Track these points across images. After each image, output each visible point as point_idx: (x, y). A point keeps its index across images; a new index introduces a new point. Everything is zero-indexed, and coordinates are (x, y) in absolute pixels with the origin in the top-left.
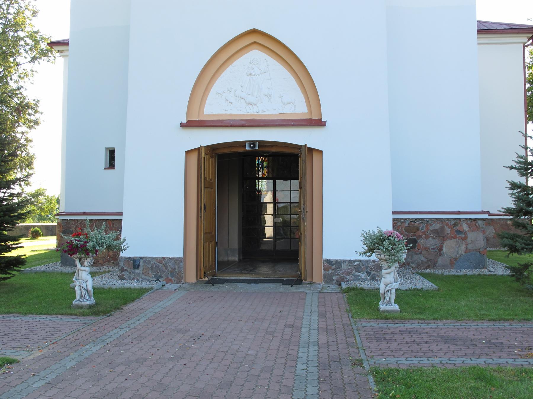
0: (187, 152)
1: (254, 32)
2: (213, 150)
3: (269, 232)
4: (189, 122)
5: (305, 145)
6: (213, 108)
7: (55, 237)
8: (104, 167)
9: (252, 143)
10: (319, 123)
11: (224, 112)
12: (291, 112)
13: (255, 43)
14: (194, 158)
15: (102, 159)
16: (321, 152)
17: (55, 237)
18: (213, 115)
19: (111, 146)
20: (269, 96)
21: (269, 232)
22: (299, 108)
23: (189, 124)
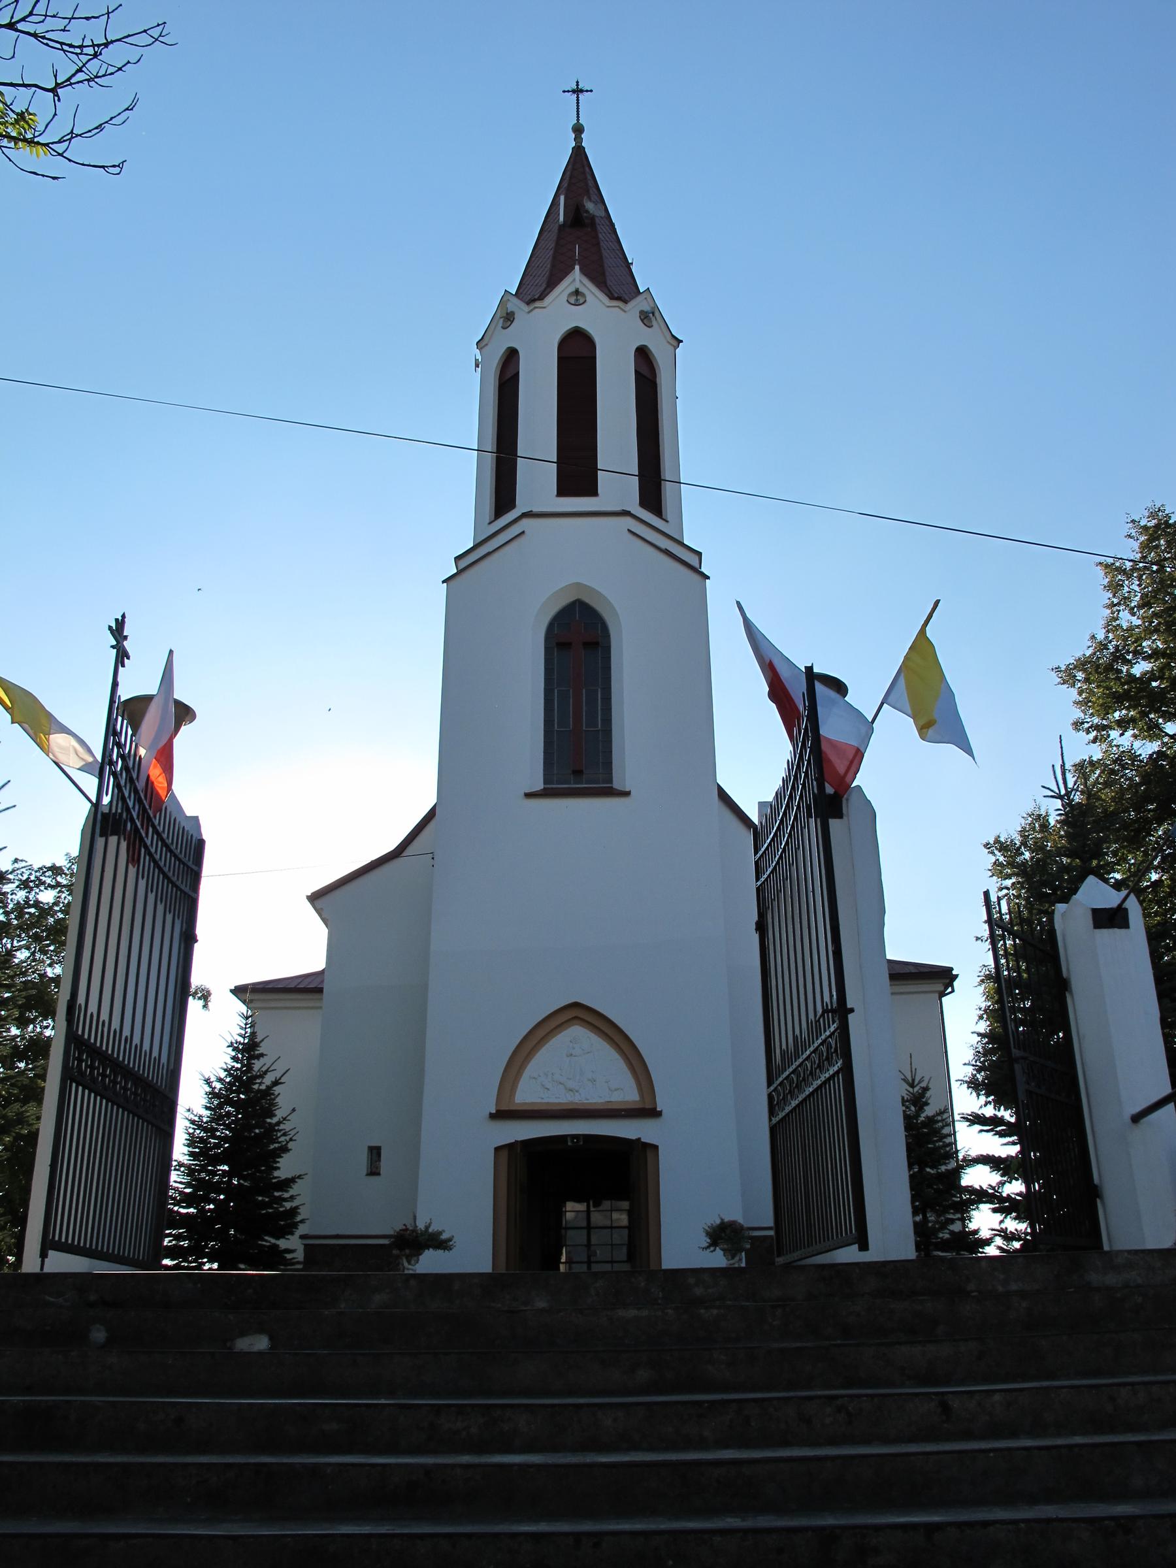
0: (497, 1149)
1: (576, 1005)
2: (528, 1145)
3: (192, 1210)
4: (498, 1111)
5: (639, 1139)
6: (527, 1094)
7: (910, 1253)
8: (365, 1172)
9: (574, 1136)
10: (653, 1113)
11: (539, 1101)
12: (619, 1099)
13: (576, 1018)
14: (504, 1154)
15: (363, 1157)
16: (655, 1148)
17: (910, 1253)
18: (525, 1104)
19: (374, 1144)
20: (593, 1081)
21: (192, 1210)
22: (627, 1093)
23: (501, 1115)
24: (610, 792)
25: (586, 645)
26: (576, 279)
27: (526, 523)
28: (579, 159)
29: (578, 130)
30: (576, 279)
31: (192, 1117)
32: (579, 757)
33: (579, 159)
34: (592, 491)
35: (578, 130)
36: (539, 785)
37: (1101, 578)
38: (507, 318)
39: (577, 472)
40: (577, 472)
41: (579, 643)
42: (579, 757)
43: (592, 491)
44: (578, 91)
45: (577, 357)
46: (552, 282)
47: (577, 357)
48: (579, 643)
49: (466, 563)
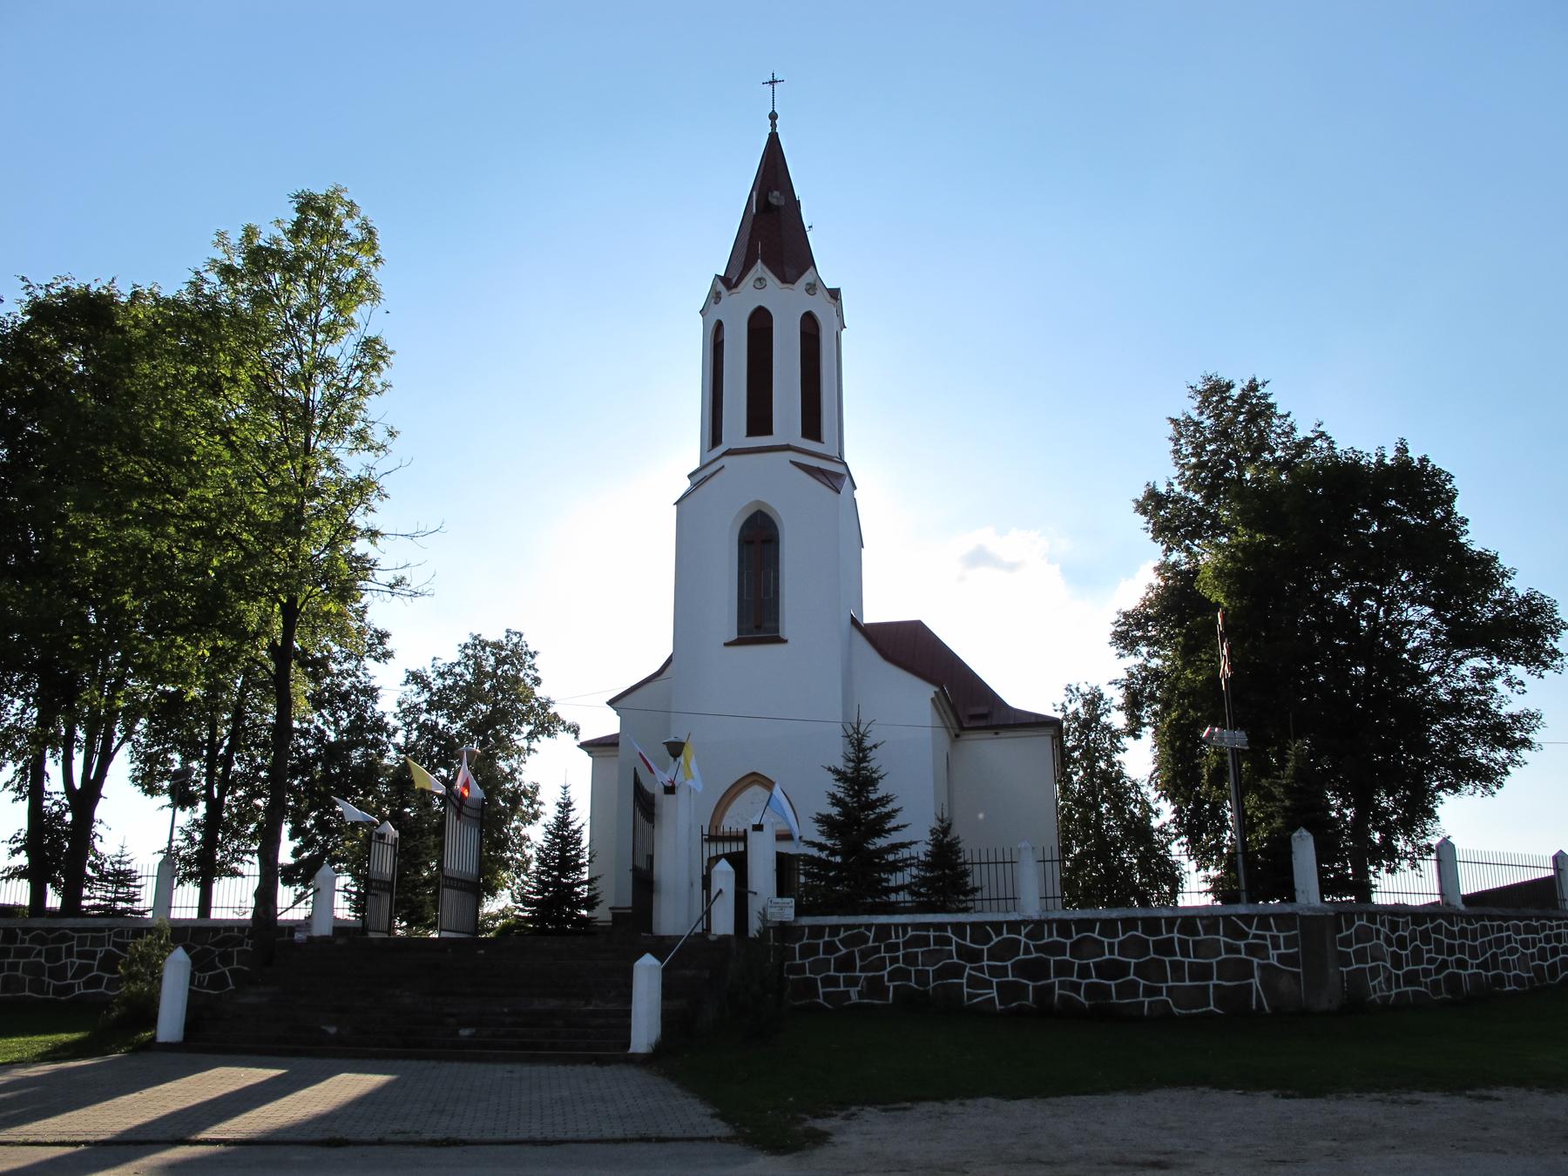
1: (754, 774)
23: (713, 838)
24: (780, 640)
25: (763, 542)
26: (759, 269)
27: (726, 460)
28: (774, 142)
29: (773, 116)
30: (759, 269)
31: (978, 895)
32: (759, 619)
33: (774, 142)
34: (769, 432)
35: (773, 116)
36: (734, 636)
37: (1170, 430)
38: (715, 296)
39: (760, 421)
40: (760, 421)
41: (759, 540)
42: (759, 619)
43: (769, 432)
44: (773, 82)
45: (760, 326)
46: (747, 266)
47: (760, 326)
48: (759, 540)
49: (699, 479)
